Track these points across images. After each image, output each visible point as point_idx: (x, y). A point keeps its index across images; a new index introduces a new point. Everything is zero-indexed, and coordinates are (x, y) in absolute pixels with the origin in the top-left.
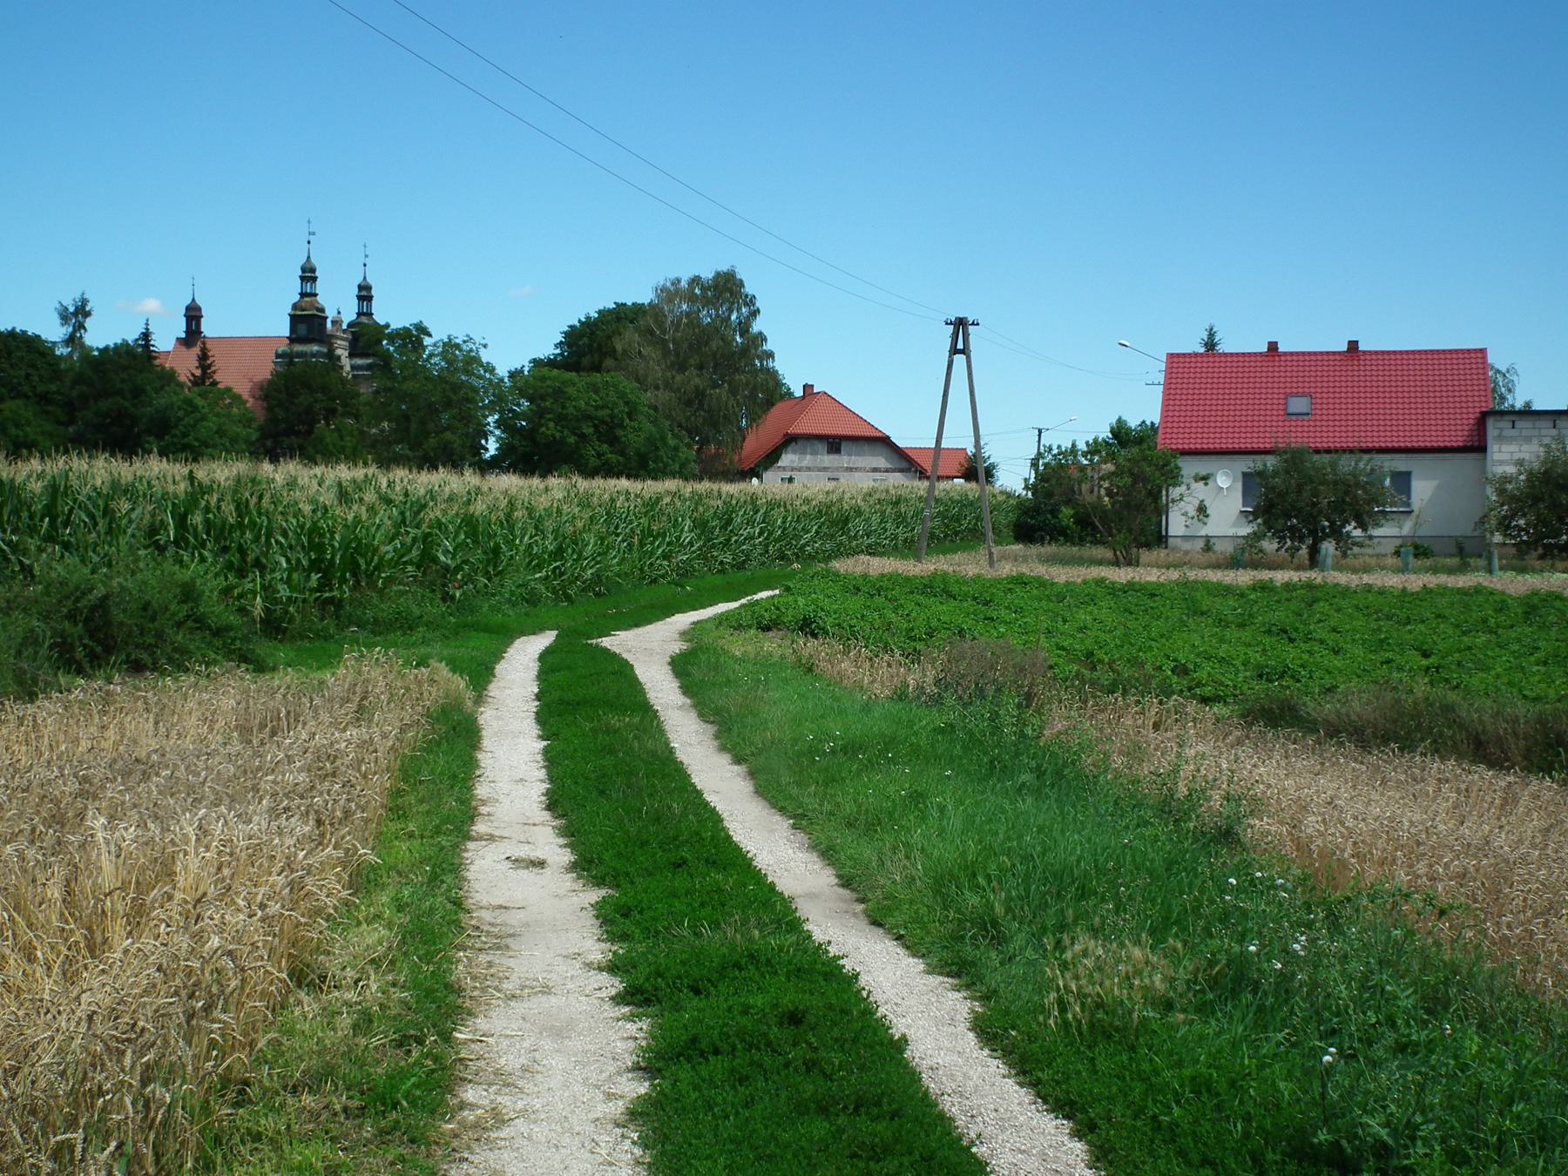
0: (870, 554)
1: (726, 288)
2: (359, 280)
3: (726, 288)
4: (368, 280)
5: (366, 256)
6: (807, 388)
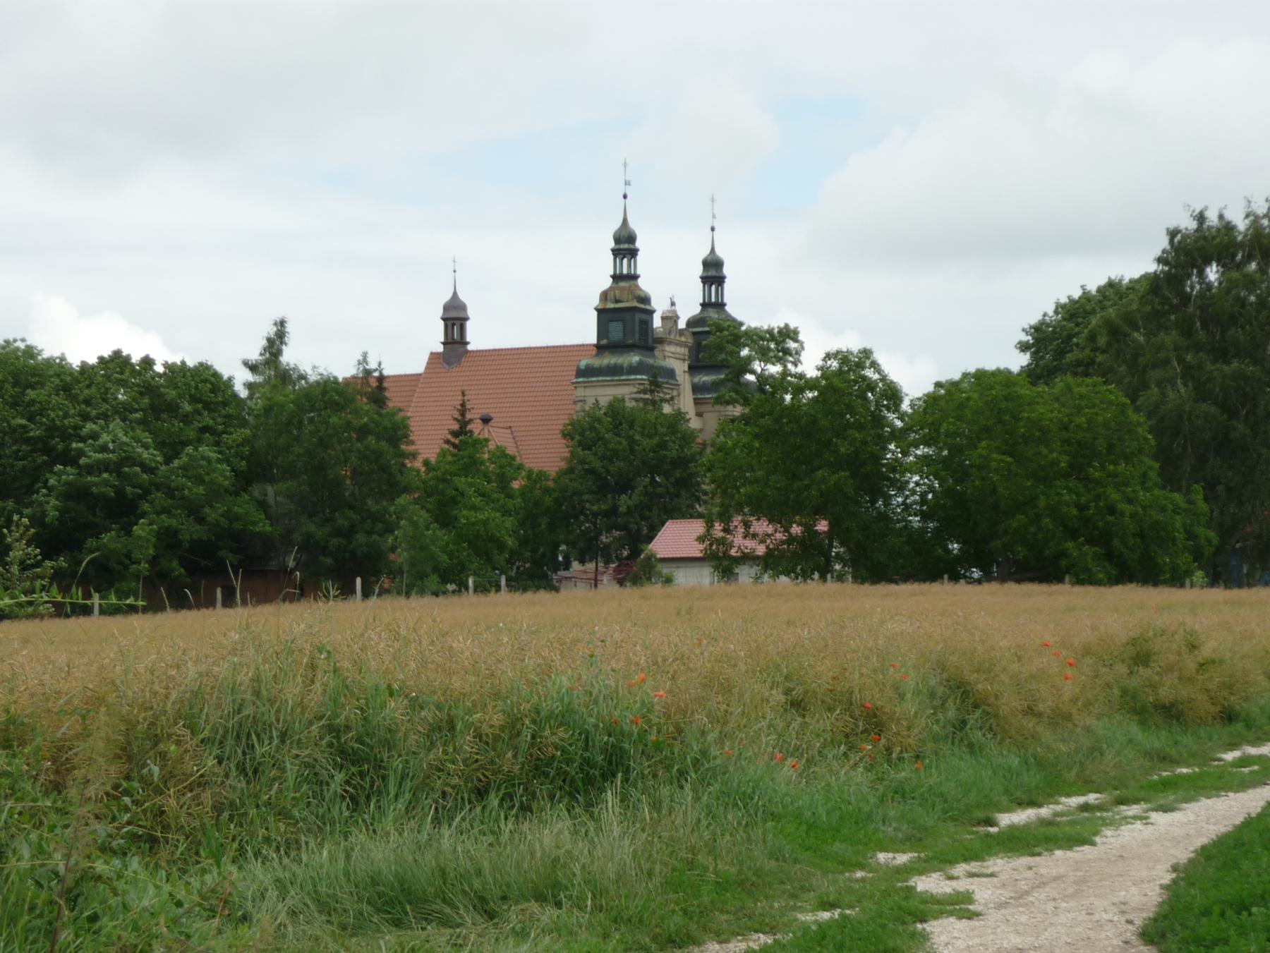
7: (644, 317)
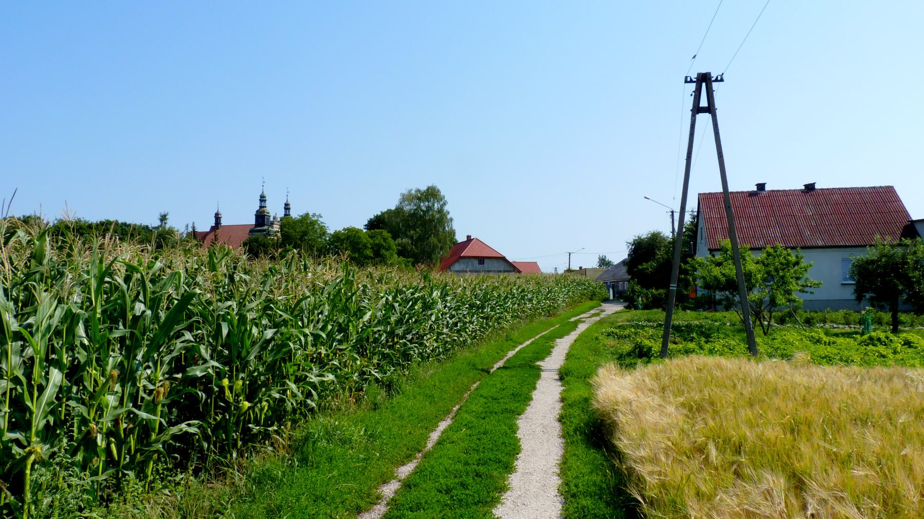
1: (432, 194)
2: (285, 202)
3: (432, 194)
4: (264, 193)
5: (288, 192)
6: (469, 237)
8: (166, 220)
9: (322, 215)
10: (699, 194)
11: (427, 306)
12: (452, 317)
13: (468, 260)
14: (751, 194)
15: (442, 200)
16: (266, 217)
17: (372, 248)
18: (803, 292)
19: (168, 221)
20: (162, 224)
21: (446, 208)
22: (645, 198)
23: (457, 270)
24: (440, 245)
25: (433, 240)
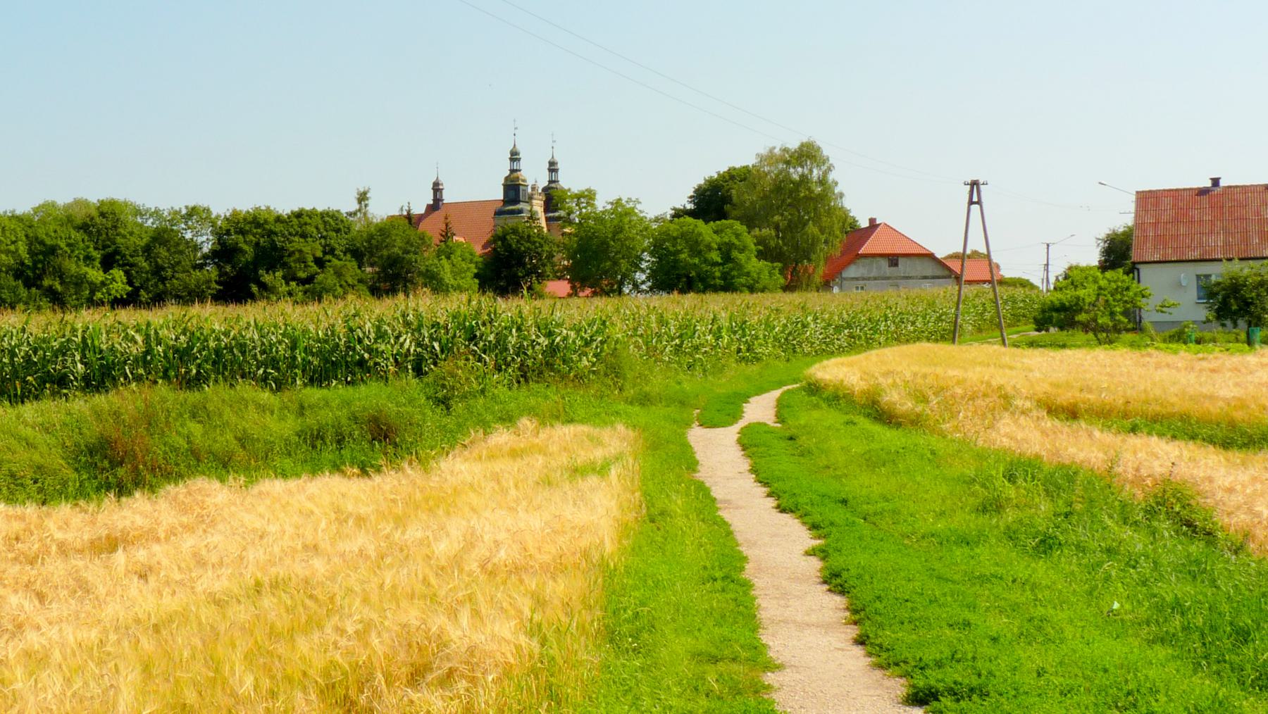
0: (1047, 491)
1: (807, 154)
2: (549, 158)
5: (554, 142)
6: (872, 221)
7: (524, 188)
8: (367, 199)
9: (640, 200)
10: (1137, 192)
11: (804, 326)
12: (821, 334)
13: (870, 259)
14: (1202, 192)
15: (824, 164)
16: (521, 188)
17: (719, 249)
18: (1162, 312)
19: (370, 202)
20: (361, 207)
21: (832, 177)
22: (1100, 183)
23: (853, 276)
24: (823, 238)
25: (812, 229)
